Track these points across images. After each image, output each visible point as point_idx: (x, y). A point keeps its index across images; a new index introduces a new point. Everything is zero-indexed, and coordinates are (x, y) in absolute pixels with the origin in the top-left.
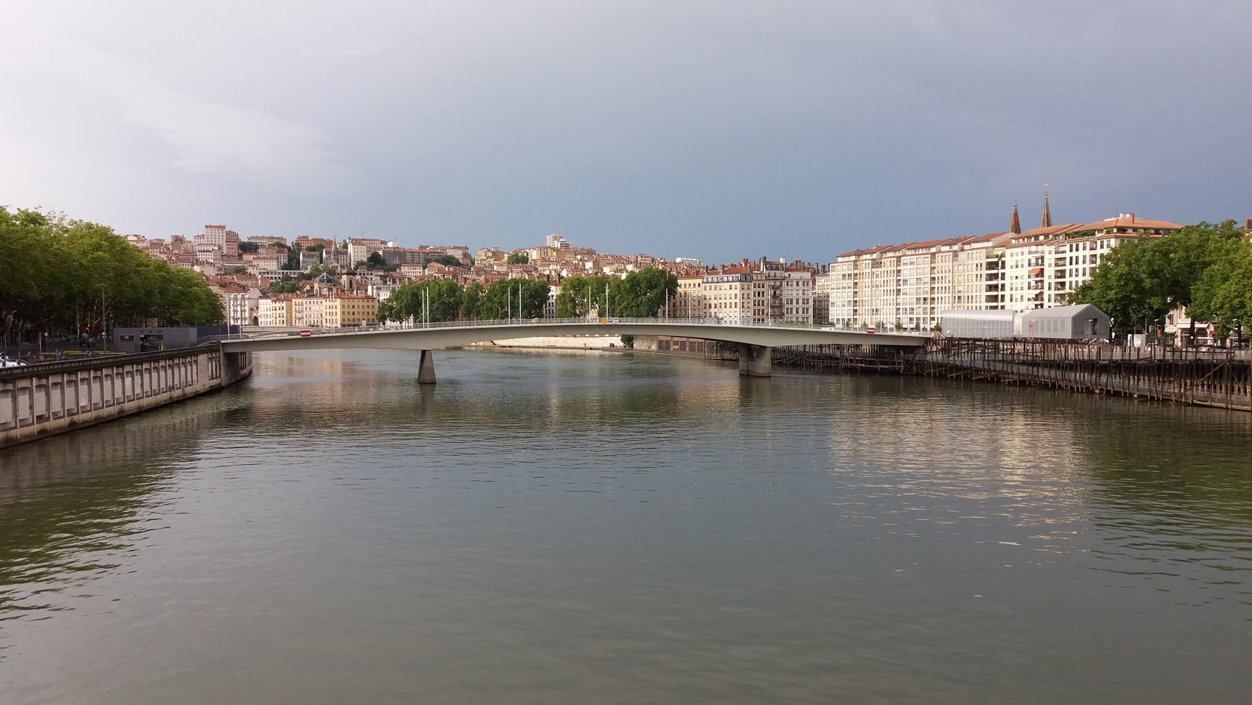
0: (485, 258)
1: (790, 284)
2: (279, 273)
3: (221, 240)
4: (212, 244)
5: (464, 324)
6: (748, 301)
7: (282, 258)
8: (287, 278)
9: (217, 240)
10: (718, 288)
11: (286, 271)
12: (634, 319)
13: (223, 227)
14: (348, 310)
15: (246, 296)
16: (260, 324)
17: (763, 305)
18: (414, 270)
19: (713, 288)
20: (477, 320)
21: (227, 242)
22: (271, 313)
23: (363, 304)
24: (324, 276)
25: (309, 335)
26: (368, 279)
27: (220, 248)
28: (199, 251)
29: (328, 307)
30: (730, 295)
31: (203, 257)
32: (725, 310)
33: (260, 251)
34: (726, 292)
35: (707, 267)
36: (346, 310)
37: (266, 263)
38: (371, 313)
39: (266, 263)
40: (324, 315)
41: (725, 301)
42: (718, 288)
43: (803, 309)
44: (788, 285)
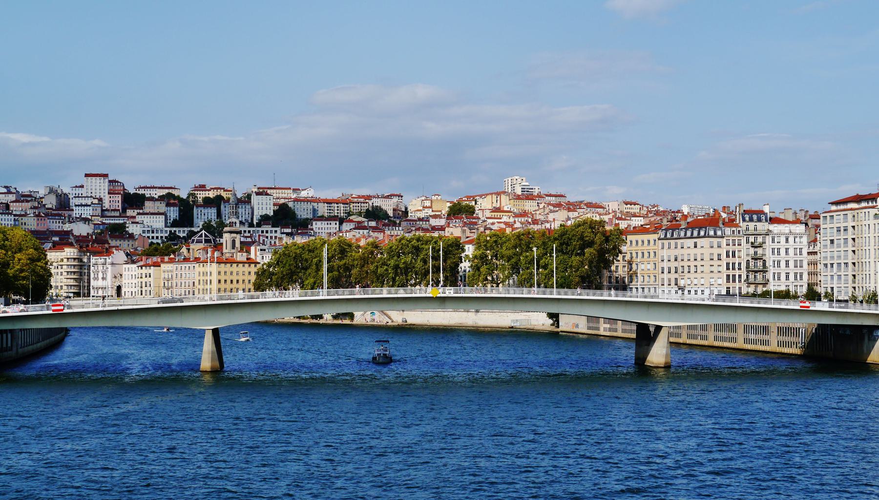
0: (421, 208)
1: (776, 241)
2: (166, 231)
3: (102, 191)
4: (91, 197)
6: (719, 263)
9: (98, 191)
10: (679, 246)
11: (174, 229)
12: (569, 291)
13: (106, 176)
14: (244, 277)
15: (109, 261)
16: (123, 294)
17: (740, 269)
18: (329, 226)
19: (673, 246)
20: (465, 286)
21: (109, 193)
22: (136, 281)
23: (244, 269)
24: (202, 234)
25: (62, 310)
27: (659, 239)
29: (201, 274)
30: (695, 255)
31: (86, 212)
33: (147, 204)
34: (689, 251)
35: (807, 211)
36: (223, 278)
37: (152, 219)
38: (247, 281)
40: (196, 284)
41: (689, 263)
42: (679, 246)
43: (796, 274)
44: (773, 241)
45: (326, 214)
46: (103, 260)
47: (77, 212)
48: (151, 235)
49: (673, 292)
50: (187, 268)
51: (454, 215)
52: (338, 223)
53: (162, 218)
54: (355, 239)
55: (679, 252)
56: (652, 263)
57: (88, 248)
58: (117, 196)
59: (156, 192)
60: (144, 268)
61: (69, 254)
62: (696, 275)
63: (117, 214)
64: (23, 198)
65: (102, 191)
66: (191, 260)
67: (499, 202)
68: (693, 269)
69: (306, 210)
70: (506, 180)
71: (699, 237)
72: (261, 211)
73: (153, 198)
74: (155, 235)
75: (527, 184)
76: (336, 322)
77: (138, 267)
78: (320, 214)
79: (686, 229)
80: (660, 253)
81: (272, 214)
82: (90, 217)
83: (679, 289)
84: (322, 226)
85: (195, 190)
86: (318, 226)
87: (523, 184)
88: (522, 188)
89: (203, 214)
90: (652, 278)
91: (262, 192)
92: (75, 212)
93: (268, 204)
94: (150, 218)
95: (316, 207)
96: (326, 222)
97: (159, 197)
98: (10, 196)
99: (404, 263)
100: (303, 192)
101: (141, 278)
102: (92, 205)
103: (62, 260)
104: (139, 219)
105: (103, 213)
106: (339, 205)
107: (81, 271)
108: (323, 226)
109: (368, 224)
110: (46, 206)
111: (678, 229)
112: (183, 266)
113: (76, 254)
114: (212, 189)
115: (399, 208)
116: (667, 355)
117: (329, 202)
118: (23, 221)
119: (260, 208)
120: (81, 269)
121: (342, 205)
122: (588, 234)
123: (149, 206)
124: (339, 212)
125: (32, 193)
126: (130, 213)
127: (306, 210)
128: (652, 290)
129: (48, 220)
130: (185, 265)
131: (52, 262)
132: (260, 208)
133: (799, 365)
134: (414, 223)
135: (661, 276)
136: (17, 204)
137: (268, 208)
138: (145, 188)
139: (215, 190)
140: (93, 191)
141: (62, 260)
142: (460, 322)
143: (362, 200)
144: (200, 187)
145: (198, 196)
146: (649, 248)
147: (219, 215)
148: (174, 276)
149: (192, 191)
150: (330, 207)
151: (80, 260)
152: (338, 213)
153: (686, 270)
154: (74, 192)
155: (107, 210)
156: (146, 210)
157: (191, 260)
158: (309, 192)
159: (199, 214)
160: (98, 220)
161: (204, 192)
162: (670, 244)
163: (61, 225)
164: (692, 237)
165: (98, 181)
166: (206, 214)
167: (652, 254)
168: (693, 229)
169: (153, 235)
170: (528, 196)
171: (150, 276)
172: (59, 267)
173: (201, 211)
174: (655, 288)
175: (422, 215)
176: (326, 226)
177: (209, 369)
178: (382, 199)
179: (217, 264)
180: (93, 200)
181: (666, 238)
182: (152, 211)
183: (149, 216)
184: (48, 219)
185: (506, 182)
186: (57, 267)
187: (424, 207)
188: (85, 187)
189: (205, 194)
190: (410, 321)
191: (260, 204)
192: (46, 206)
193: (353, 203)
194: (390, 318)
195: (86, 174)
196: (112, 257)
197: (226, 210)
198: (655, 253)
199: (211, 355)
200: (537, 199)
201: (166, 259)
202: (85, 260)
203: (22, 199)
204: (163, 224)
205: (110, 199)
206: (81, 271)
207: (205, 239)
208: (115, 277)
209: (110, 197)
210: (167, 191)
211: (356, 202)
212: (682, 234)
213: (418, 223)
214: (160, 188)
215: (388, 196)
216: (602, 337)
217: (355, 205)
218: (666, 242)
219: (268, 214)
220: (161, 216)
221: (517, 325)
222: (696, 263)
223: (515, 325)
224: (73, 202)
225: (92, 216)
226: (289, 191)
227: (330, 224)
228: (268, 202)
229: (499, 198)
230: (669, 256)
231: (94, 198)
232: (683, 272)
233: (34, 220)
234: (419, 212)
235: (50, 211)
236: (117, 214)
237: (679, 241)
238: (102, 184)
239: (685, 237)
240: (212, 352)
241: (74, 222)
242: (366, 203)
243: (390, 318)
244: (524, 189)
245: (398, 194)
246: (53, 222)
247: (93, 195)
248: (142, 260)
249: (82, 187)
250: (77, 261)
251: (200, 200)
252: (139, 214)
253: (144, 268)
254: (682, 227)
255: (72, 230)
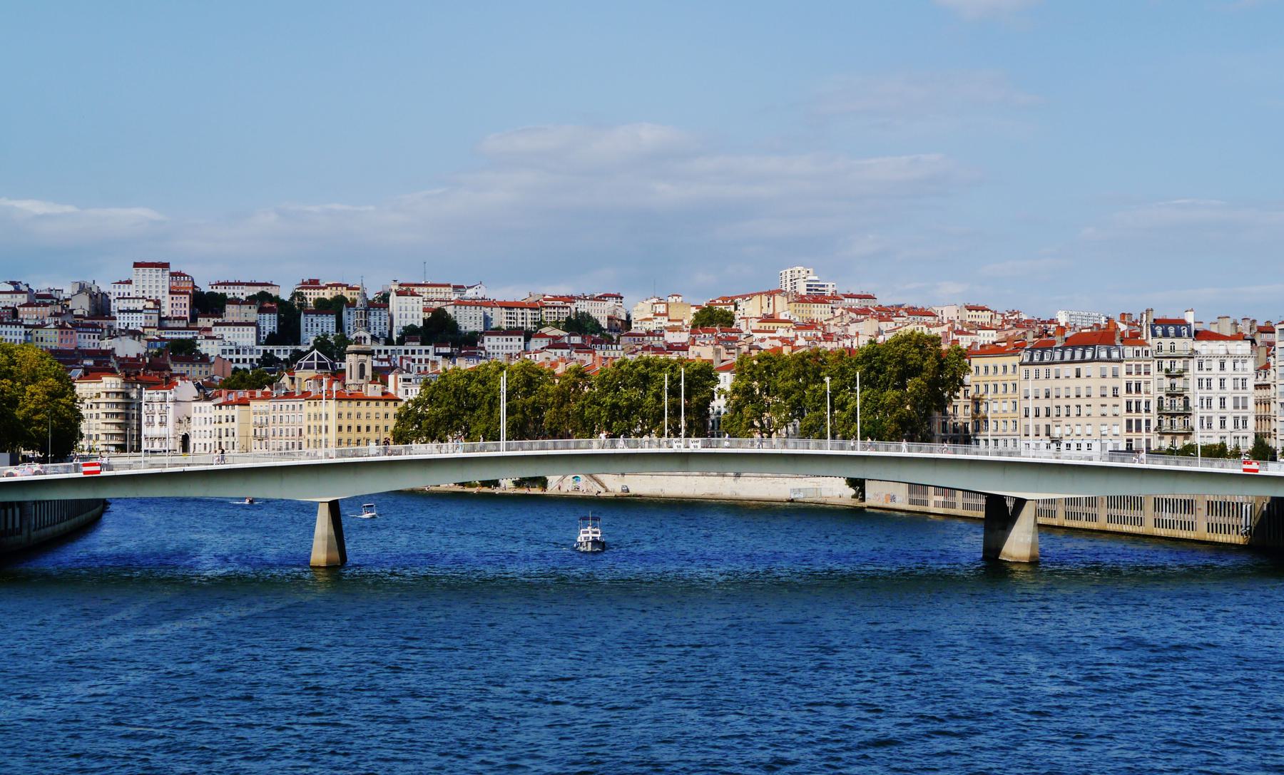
2: (258, 351)
3: (160, 289)
5: (572, 445)
6: (1116, 401)
7: (267, 322)
8: (268, 360)
10: (1052, 375)
13: (165, 266)
15: (170, 396)
18: (509, 343)
21: (171, 293)
24: (313, 355)
25: (1257, 471)
26: (413, 361)
27: (1021, 364)
28: (120, 311)
29: (312, 417)
31: (134, 321)
32: (1065, 420)
33: (230, 309)
35: (1254, 321)
37: (236, 332)
38: (382, 429)
39: (236, 332)
40: (305, 431)
41: (1067, 402)
42: (1052, 375)
45: (505, 325)
46: (161, 396)
47: (122, 322)
48: (234, 356)
49: (1043, 446)
50: (291, 407)
51: (702, 326)
52: (522, 338)
53: (252, 330)
54: (549, 363)
55: (1052, 384)
56: (1010, 401)
57: (138, 377)
58: (183, 296)
59: (243, 291)
60: (224, 407)
61: (108, 386)
62: (1079, 420)
63: (184, 324)
64: (38, 300)
65: (160, 289)
66: (297, 395)
67: (771, 306)
68: (1074, 411)
69: (473, 318)
70: (783, 272)
71: (1083, 361)
72: (403, 319)
73: (239, 299)
74: (241, 357)
75: (816, 278)
76: (519, 491)
77: (215, 405)
78: (495, 325)
79: (1064, 348)
80: (1023, 386)
81: (421, 324)
82: (141, 330)
83: (1053, 442)
84: (498, 344)
85: (302, 288)
86: (491, 343)
87: (809, 278)
88: (808, 285)
89: (315, 325)
90: (1011, 425)
91: (406, 291)
92: (118, 321)
93: (415, 309)
94: (234, 330)
95: (489, 314)
96: (504, 338)
97: (247, 298)
98: (20, 296)
99: (627, 399)
100: (468, 291)
101: (220, 422)
102: (145, 311)
103: (98, 395)
104: (216, 331)
105: (162, 323)
106: (525, 311)
107: (128, 411)
108: (500, 343)
109: (569, 340)
110: (75, 313)
111: (1051, 349)
112: (284, 404)
113: (119, 386)
114: (328, 285)
115: (617, 316)
116: (1033, 545)
117: (509, 306)
118: (39, 335)
119: (403, 316)
120: (127, 409)
121: (529, 311)
122: (914, 356)
123: (232, 312)
124: (524, 321)
125: (53, 293)
126: (203, 322)
127: (473, 318)
128: (1010, 443)
129: (78, 334)
130: (288, 403)
131: (84, 399)
132: (403, 316)
133: (1244, 560)
134: (641, 338)
135: (1025, 421)
136: (30, 309)
137: (415, 316)
138: (226, 284)
139: (334, 288)
140: (147, 289)
141: (98, 395)
142: (711, 492)
143: (560, 303)
144: (310, 284)
145: (308, 297)
146: (1004, 377)
147: (340, 325)
148: (271, 420)
149: (299, 289)
150: (511, 313)
151: (126, 395)
152: (523, 323)
153: (1064, 412)
154: (117, 290)
155: (167, 318)
156: (228, 319)
157: (297, 395)
158: (478, 291)
159: (309, 325)
160: (153, 334)
161: (316, 291)
162: (1037, 372)
163: (97, 341)
164: (1072, 362)
165: (154, 274)
166: (320, 325)
167: (1010, 388)
168: (1074, 348)
169: (238, 356)
170: (816, 297)
171: (233, 420)
172: (94, 406)
173: (312, 320)
174: (1015, 440)
175: (652, 326)
176: (505, 343)
177: (323, 564)
178: (590, 302)
179: (337, 402)
180: (146, 303)
181: (1031, 363)
182: (236, 320)
183: (232, 328)
184: (77, 332)
185: (783, 276)
186: (91, 406)
187: (655, 314)
188: (134, 282)
189: (318, 294)
190: (633, 491)
191: (403, 309)
192: (75, 313)
193: (547, 307)
194: (603, 486)
195: (135, 263)
196: (175, 391)
197: (350, 318)
198: (1015, 385)
199: (326, 542)
200: (831, 301)
201: (258, 393)
202: (134, 395)
203: (37, 301)
204: (254, 339)
205: (173, 302)
206: (128, 411)
207: (318, 364)
208: (180, 422)
209: (173, 299)
210: (259, 289)
211: (551, 307)
212: (1057, 356)
213: (646, 338)
214: (248, 284)
215: (601, 297)
216: (932, 517)
217: (549, 310)
218: (1032, 369)
219: (415, 324)
220: (250, 328)
221: (800, 496)
222: (1078, 401)
223: (796, 496)
224: (116, 305)
225: (144, 327)
226: (447, 289)
227: (511, 340)
228: (416, 306)
229: (771, 301)
230: (1037, 391)
231: (147, 300)
232: (1068, 415)
233: (56, 333)
234: (648, 322)
235: (80, 319)
236: (184, 324)
237: (1053, 368)
238: (160, 279)
239: (1062, 362)
240: (329, 537)
241: (117, 336)
242: (567, 307)
243: (603, 486)
244: (811, 286)
245: (616, 293)
246: (85, 337)
247: (147, 295)
248: (221, 396)
249: (129, 282)
250: (120, 396)
251: (311, 303)
252: (216, 324)
253: (224, 407)
254: (1057, 345)
255: (113, 349)
